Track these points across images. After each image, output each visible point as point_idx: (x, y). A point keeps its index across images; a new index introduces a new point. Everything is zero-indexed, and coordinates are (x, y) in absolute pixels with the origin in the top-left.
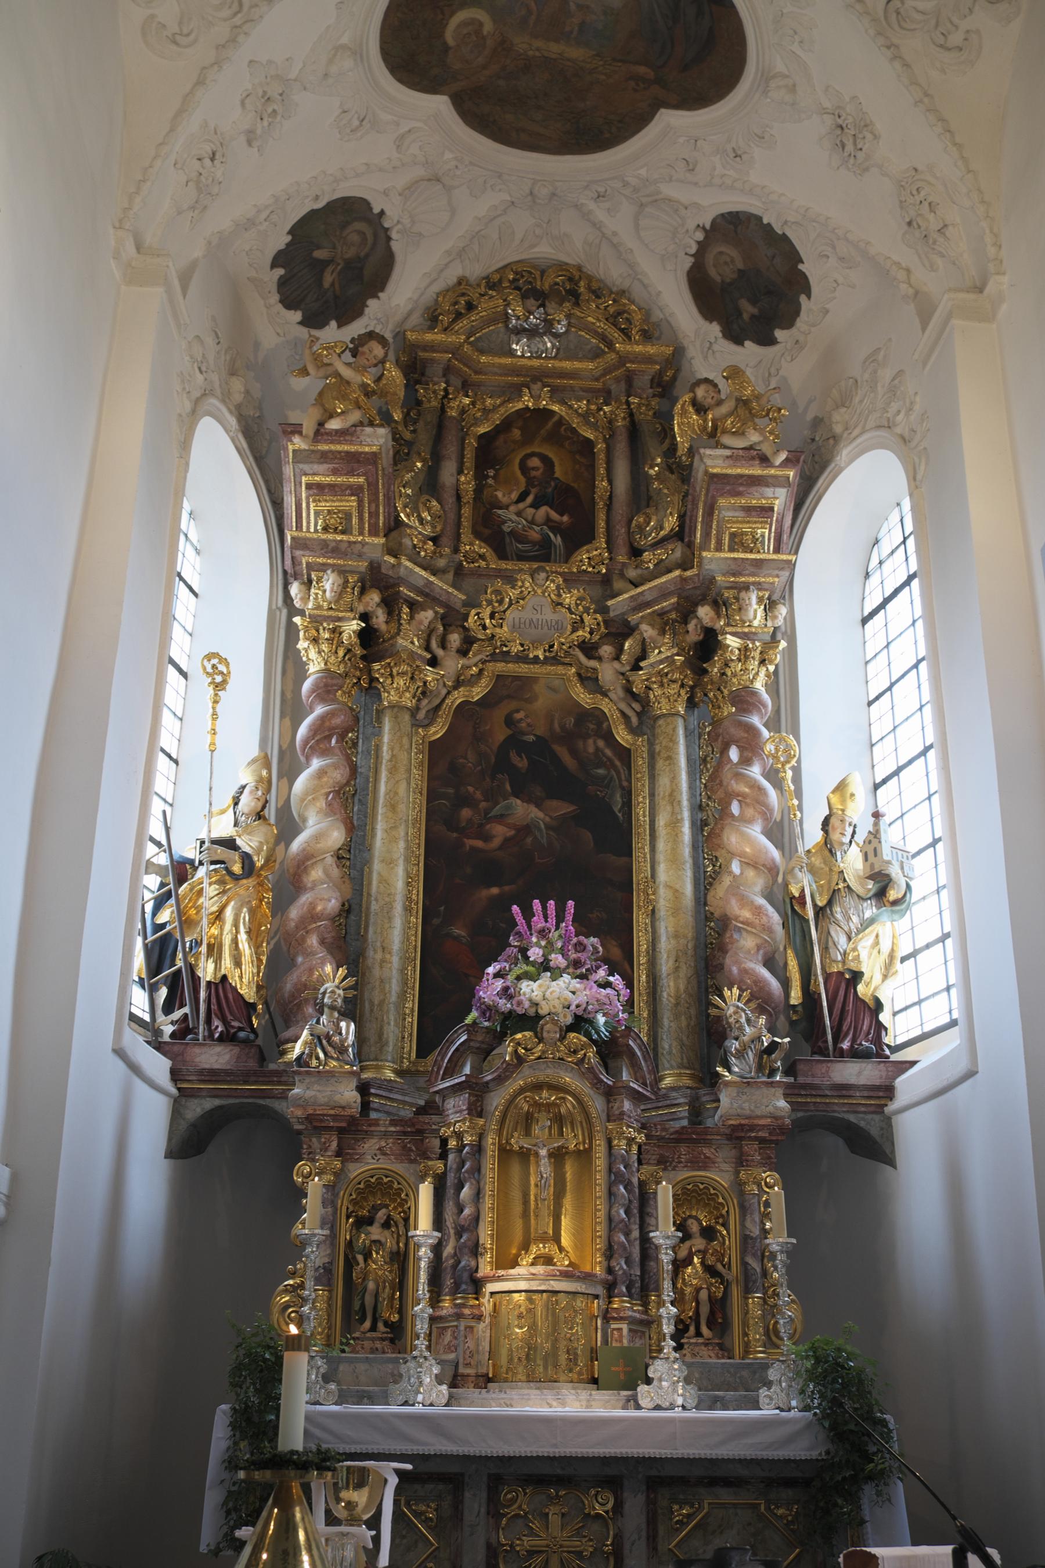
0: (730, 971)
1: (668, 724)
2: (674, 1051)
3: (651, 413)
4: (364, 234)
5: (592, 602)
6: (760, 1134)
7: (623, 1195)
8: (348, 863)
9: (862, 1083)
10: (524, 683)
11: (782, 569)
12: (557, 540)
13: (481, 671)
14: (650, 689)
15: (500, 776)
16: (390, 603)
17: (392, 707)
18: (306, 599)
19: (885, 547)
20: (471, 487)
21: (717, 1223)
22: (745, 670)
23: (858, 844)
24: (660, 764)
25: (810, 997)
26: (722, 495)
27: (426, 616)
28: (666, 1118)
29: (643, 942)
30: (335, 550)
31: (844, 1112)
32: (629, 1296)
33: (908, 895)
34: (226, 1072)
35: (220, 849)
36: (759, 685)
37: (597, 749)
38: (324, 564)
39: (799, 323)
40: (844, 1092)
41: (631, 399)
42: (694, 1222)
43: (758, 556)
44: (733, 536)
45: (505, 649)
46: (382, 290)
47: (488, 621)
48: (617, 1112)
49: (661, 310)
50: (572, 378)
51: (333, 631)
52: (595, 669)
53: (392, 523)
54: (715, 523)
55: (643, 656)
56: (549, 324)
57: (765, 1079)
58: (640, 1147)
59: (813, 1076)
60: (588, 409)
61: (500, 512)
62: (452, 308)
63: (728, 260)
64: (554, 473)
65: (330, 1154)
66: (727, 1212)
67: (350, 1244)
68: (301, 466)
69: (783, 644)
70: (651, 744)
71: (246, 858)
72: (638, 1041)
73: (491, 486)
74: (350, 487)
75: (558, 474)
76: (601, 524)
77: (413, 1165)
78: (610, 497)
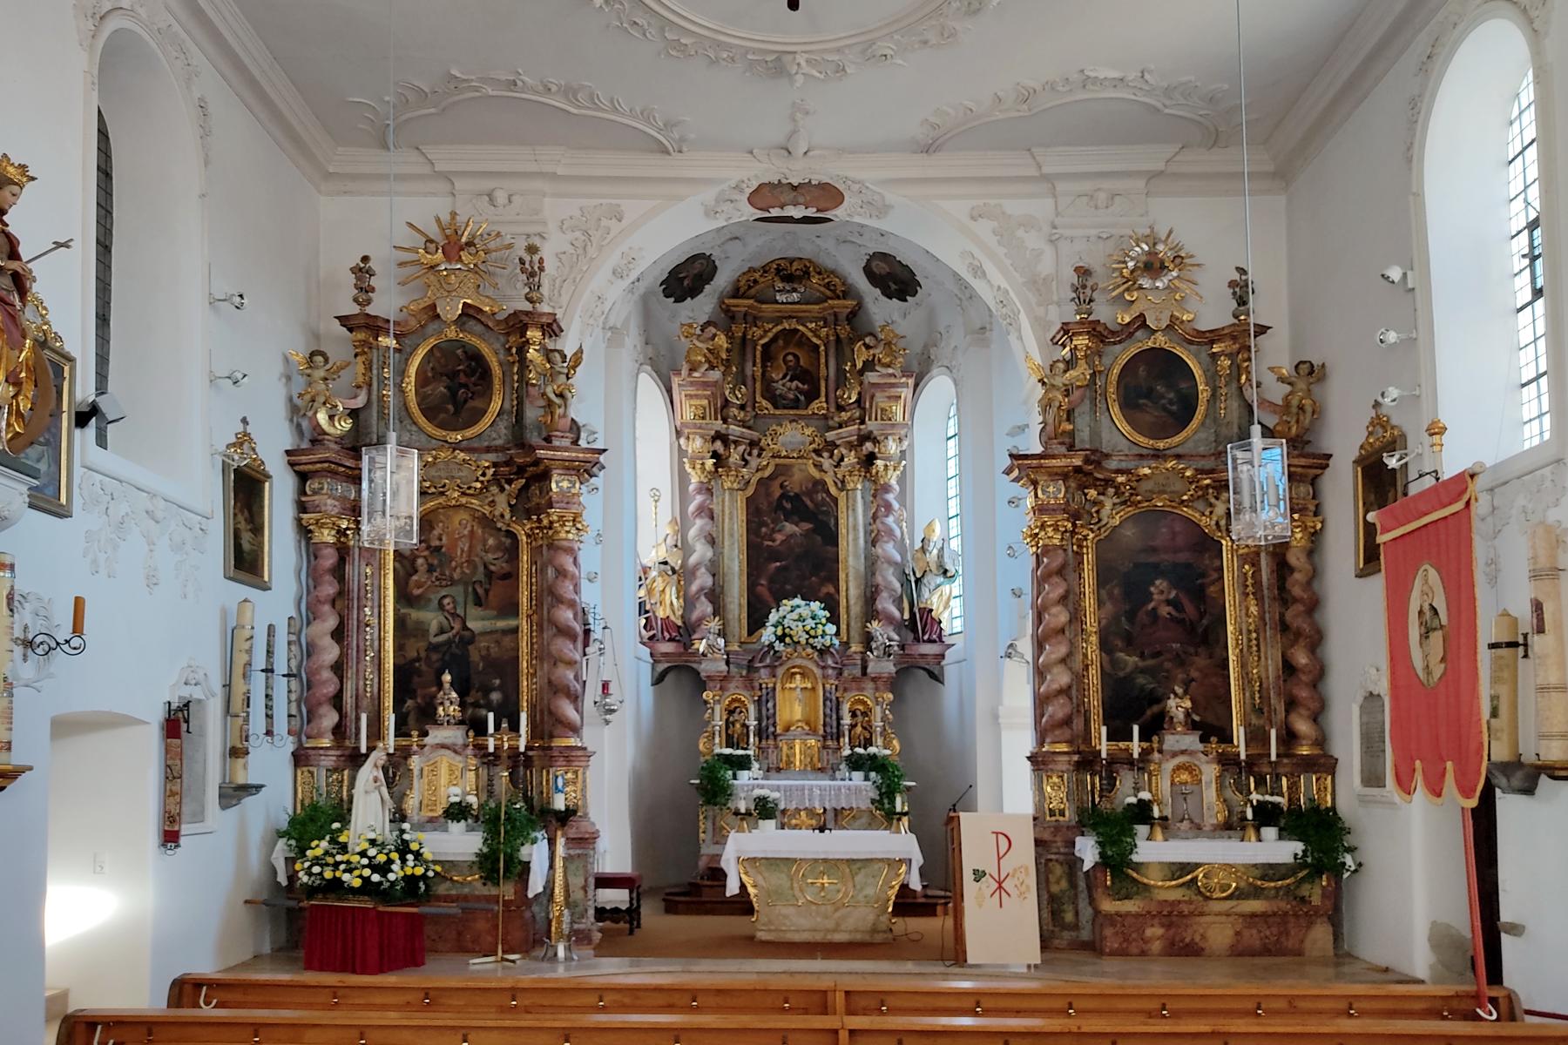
10: (788, 467)
12: (802, 398)
17: (729, 489)
20: (759, 374)
22: (886, 474)
36: (893, 482)
75: (802, 363)
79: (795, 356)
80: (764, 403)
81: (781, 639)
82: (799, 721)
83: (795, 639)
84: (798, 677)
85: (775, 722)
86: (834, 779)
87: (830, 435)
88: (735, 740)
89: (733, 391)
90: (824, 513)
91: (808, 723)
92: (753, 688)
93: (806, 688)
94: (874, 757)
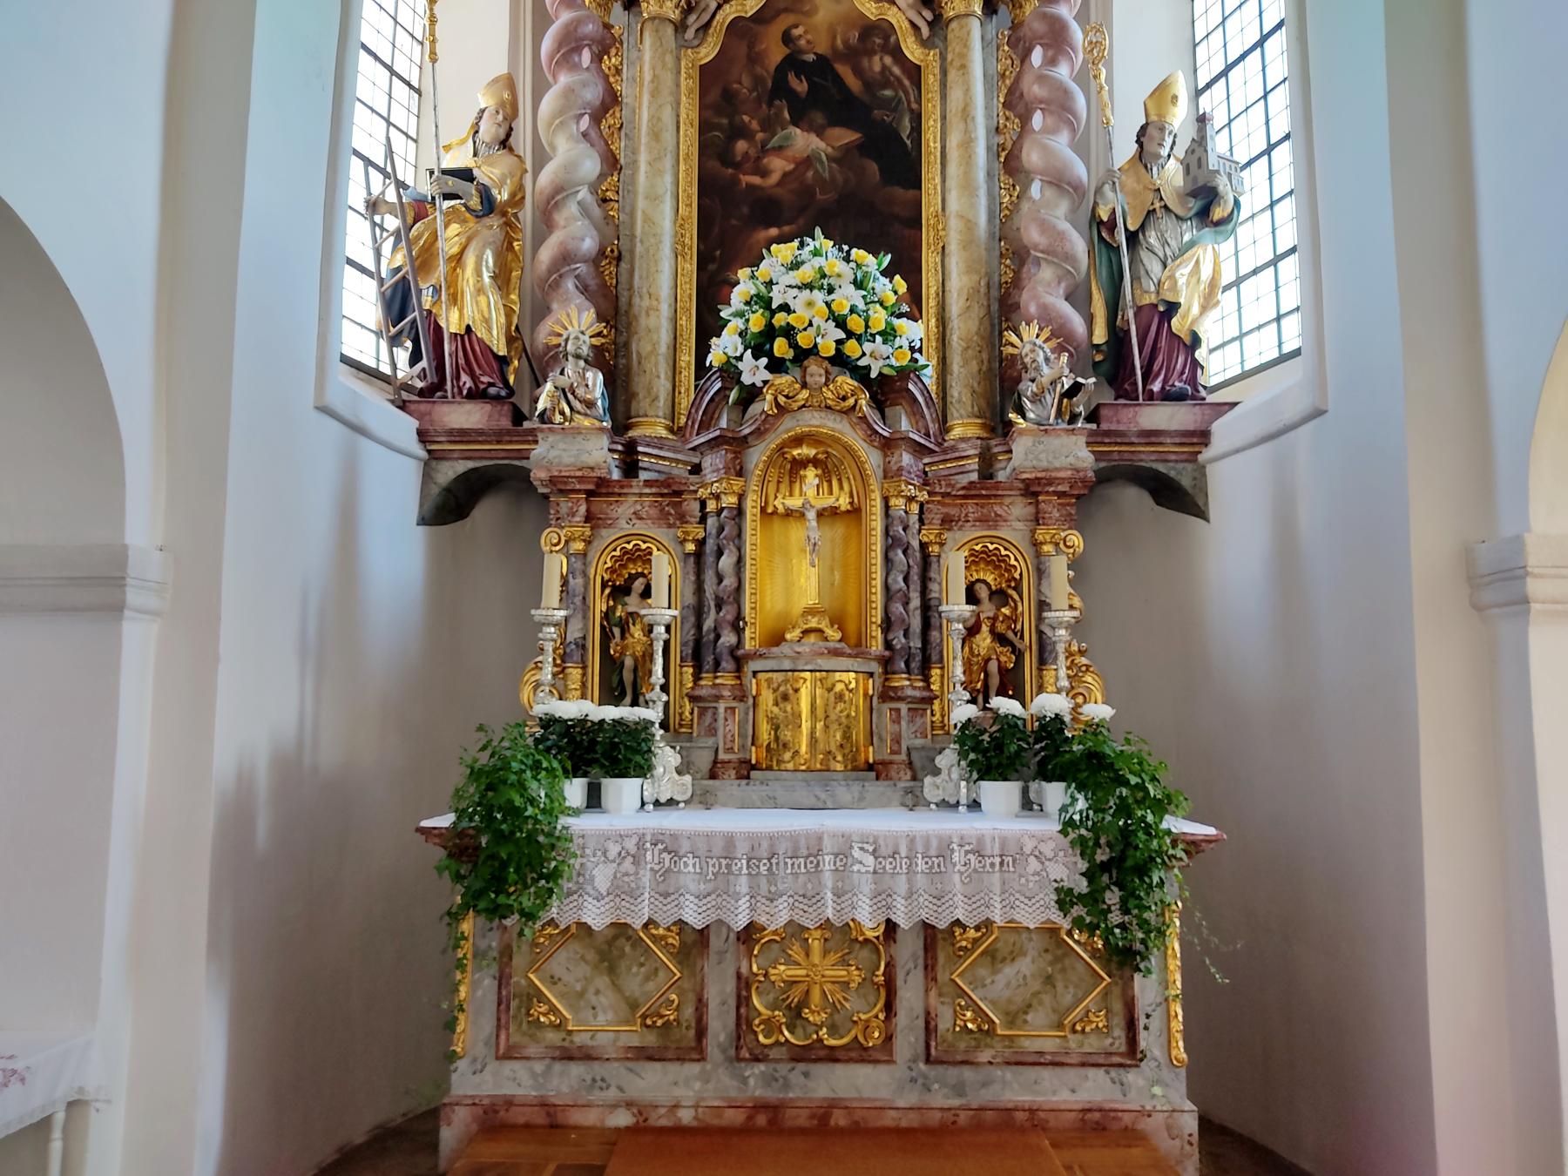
1: (962, 27)
2: (964, 399)
6: (1060, 488)
7: (901, 561)
8: (616, 206)
9: (1173, 428)
15: (777, 102)
17: (652, 19)
21: (1009, 586)
23: (1177, 159)
25: (1118, 337)
28: (953, 471)
31: (1153, 461)
32: (908, 672)
34: (480, 432)
35: (451, 181)
37: (884, 67)
40: (1153, 439)
42: (983, 586)
48: (895, 468)
57: (1065, 426)
58: (922, 505)
59: (1118, 422)
65: (578, 519)
66: (1021, 574)
67: (607, 615)
70: (943, 57)
71: (485, 195)
72: (920, 384)
77: (672, 530)
81: (760, 345)
82: (810, 612)
83: (803, 340)
84: (811, 474)
85: (739, 616)
86: (915, 800)
90: (886, 104)
91: (838, 621)
92: (682, 518)
94: (1051, 728)
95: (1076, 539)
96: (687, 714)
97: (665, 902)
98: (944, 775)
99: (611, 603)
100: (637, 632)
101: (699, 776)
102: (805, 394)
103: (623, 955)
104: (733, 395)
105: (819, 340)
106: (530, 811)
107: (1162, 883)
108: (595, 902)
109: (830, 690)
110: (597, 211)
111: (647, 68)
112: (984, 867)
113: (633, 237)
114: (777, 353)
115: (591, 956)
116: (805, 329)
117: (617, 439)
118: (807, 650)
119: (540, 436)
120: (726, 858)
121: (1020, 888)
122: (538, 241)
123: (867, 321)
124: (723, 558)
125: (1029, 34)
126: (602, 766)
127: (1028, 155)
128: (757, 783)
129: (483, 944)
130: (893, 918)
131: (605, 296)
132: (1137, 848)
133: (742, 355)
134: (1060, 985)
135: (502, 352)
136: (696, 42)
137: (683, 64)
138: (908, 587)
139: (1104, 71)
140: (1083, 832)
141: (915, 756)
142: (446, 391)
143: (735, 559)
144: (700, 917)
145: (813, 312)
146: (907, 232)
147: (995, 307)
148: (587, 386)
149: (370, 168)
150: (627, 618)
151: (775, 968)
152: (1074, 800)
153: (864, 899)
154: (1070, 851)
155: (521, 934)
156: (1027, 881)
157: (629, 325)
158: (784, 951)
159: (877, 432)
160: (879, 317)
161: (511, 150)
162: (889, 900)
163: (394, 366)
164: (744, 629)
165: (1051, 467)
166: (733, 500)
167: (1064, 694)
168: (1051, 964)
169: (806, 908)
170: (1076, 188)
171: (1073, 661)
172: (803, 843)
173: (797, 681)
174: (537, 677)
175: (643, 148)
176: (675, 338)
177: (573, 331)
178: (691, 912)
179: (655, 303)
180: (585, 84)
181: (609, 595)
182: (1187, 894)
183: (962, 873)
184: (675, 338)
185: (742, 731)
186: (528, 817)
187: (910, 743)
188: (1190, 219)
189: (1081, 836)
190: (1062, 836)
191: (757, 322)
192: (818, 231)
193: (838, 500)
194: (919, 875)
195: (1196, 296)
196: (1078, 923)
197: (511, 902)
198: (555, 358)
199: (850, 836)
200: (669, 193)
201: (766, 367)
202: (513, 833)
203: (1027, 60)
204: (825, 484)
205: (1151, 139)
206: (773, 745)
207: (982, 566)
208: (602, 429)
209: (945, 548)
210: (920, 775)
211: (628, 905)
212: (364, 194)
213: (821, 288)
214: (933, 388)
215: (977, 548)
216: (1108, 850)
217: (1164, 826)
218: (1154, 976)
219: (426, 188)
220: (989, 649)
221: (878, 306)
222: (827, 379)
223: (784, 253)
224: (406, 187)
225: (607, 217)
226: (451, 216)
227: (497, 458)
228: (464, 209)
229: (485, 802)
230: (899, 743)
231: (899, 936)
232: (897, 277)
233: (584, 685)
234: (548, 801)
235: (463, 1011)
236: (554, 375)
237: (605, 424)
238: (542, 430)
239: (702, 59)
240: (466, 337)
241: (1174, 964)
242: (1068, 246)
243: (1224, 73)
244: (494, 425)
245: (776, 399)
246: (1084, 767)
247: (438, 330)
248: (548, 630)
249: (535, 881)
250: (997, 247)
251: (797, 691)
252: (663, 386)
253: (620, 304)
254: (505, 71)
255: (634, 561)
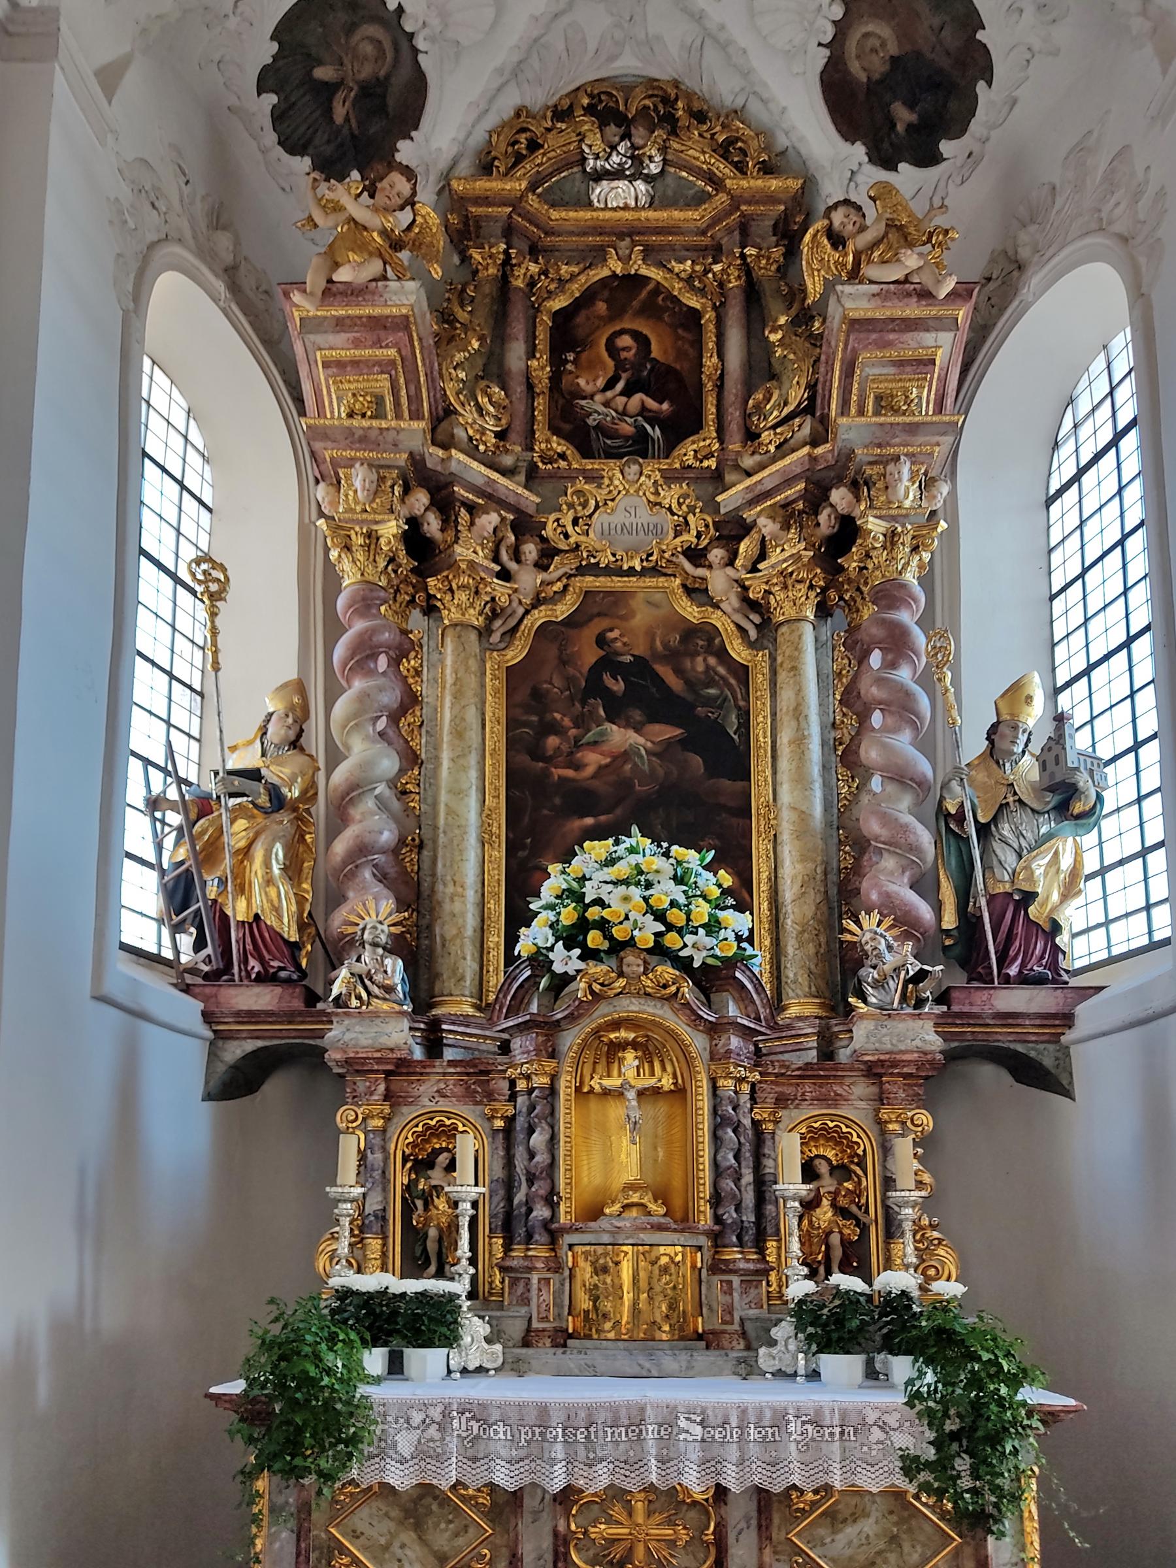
0: (868, 895)
3: (774, 268)
4: (380, 42)
5: (698, 499)
6: (905, 1070)
8: (417, 798)
10: (619, 598)
11: (944, 434)
13: (566, 587)
14: (770, 593)
15: (592, 701)
16: (443, 503)
18: (335, 504)
19: (1084, 405)
21: (852, 1162)
23: (1032, 755)
24: (782, 676)
25: (969, 923)
26: (865, 347)
27: (489, 520)
29: (764, 868)
30: (363, 440)
32: (741, 1246)
33: (1098, 806)
35: (237, 781)
36: (910, 577)
38: (352, 459)
39: (975, 126)
40: (1010, 1021)
41: (748, 251)
42: (823, 1162)
43: (916, 419)
44: (879, 398)
45: (593, 560)
46: (416, 128)
47: (570, 529)
48: (722, 1051)
49: (787, 134)
50: (670, 234)
51: (369, 535)
52: (704, 579)
53: (441, 413)
54: (855, 386)
55: (762, 556)
56: (637, 160)
57: (910, 1011)
58: (753, 1085)
59: (971, 1004)
60: (694, 271)
61: (583, 402)
62: (510, 149)
63: (877, 43)
64: (650, 352)
66: (864, 1151)
67: (409, 1188)
68: (312, 337)
69: (943, 525)
70: (773, 659)
71: (275, 793)
72: (748, 973)
73: (571, 372)
74: (378, 363)
75: (656, 352)
76: (711, 409)
77: (479, 1107)
78: (722, 375)
79: (637, 335)
80: (558, 445)
81: (572, 937)
82: (631, 1187)
83: (618, 933)
84: (630, 1058)
85: (553, 1191)
86: (748, 1369)
87: (729, 499)
88: (432, 1246)
89: (469, 391)
90: (709, 702)
91: (661, 1196)
92: (490, 1096)
93: (656, 1091)
95: (925, 1119)
96: (497, 1282)
97: (474, 1466)
98: (780, 1346)
99: (413, 1176)
100: (441, 1204)
101: (510, 1344)
102: (622, 982)
103: (430, 1512)
104: (544, 983)
105: (636, 933)
106: (326, 1381)
107: (1015, 1452)
108: (398, 1465)
109: (653, 1263)
110: (396, 805)
111: (448, 671)
112: (823, 1435)
113: (435, 828)
114: (590, 944)
115: (395, 1513)
116: (621, 923)
117: (419, 1018)
118: (628, 1225)
119: (335, 1019)
120: (539, 1427)
121: (861, 1456)
122: (333, 834)
123: (688, 914)
124: (535, 1135)
125: (866, 639)
126: (405, 1337)
127: (866, 753)
128: (575, 1351)
129: (280, 1500)
130: (723, 1483)
131: (406, 883)
132: (988, 1419)
133: (553, 946)
134: (906, 1547)
135: (294, 937)
136: (502, 645)
137: (488, 665)
138: (739, 1164)
139: (949, 674)
140: (931, 1404)
141: (749, 1326)
142: (233, 975)
143: (547, 1136)
144: (512, 1480)
145: (630, 907)
146: (734, 821)
147: (833, 891)
148: (386, 972)
149: (149, 768)
150: (431, 1191)
151: (595, 1527)
152: (922, 1374)
153: (691, 1465)
154: (917, 1421)
155: (319, 1493)
156: (870, 1449)
157: (432, 910)
158: (604, 1511)
159: (702, 1018)
160: (702, 912)
161: (302, 750)
162: (719, 1466)
163: (177, 952)
164: (558, 1203)
165: (895, 1049)
166: (545, 1080)
167: (912, 1271)
168: (896, 1524)
169: (627, 1473)
170: (919, 784)
171: (923, 1235)
172: (623, 1413)
173: (618, 1255)
174: (334, 1247)
175: (445, 746)
176: (483, 921)
177: (370, 921)
178: (502, 1476)
179: (460, 890)
180: (381, 689)
181: (411, 1169)
182: (1044, 1461)
183: (798, 1442)
184: (483, 921)
185: (558, 1300)
186: (323, 1387)
187: (743, 1313)
188: (1048, 812)
189: (928, 1407)
190: (908, 1408)
191: (568, 915)
192: (635, 829)
193: (660, 1080)
194: (751, 1444)
195: (1056, 885)
196: (925, 1487)
197: (308, 1464)
198: (352, 942)
199: (676, 1407)
200: (474, 787)
201: (579, 958)
202: (308, 1401)
203: (865, 663)
204: (646, 1065)
205: (1003, 736)
206: (592, 1315)
207: (822, 1142)
208: (403, 1013)
209: (780, 1125)
210: (754, 1344)
211: (434, 1469)
212: (144, 792)
213: (638, 884)
214: (765, 979)
215: (816, 1125)
216: (957, 1420)
217: (1019, 1397)
218: (1007, 1539)
219: (211, 786)
220: (830, 1222)
221: (700, 900)
222: (646, 969)
223: (597, 850)
224: (189, 784)
225: (407, 809)
226: (236, 814)
227: (289, 1038)
228: (251, 806)
229: (277, 1372)
230: (731, 1313)
231: (730, 1497)
232: (722, 872)
233: (384, 1254)
234: (345, 1372)
235: (260, 1562)
236: (350, 961)
237: (405, 1007)
238: (337, 1014)
239: (508, 661)
240: (254, 925)
241: (1032, 1527)
242: (912, 838)
243: (1087, 672)
244: (285, 1006)
245: (590, 986)
246: (932, 1342)
247: (225, 918)
248: (344, 1206)
249: (333, 1445)
250: (835, 834)
251: (617, 1263)
252: (469, 967)
253: (422, 889)
254: (295, 676)
255: (438, 1136)
